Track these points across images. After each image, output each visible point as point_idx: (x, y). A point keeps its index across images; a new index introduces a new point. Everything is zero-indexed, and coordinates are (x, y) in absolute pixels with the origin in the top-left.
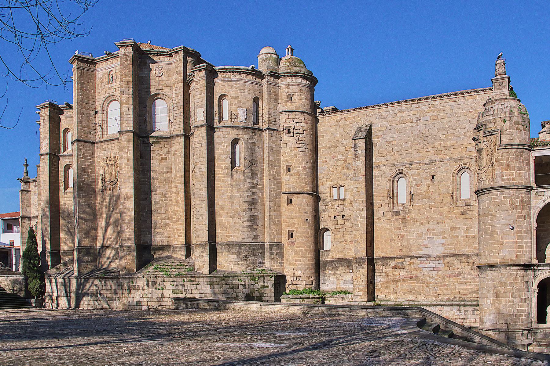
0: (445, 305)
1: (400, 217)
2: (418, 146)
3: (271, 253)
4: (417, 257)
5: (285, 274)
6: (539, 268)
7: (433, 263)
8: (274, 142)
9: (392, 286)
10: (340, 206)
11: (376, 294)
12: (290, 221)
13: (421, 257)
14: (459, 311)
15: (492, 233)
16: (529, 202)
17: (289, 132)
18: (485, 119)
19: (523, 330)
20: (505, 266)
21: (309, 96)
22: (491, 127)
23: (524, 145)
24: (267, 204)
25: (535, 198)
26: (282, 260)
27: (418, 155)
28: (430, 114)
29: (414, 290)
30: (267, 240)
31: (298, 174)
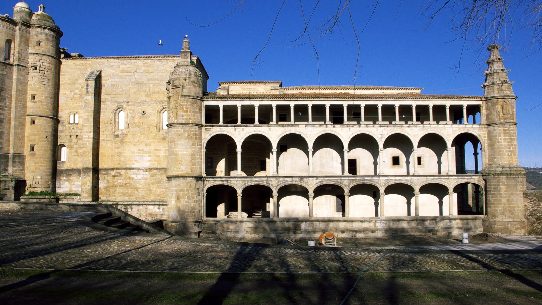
0: (149, 205)
1: (119, 139)
2: (134, 90)
3: (14, 162)
4: (131, 169)
5: (26, 179)
6: (207, 179)
7: (142, 174)
8: (22, 75)
9: (112, 190)
10: (75, 128)
11: (100, 196)
12: (32, 137)
13: (133, 169)
14: (159, 209)
15: (175, 154)
16: (201, 135)
17: (36, 69)
18: (174, 77)
19: (195, 222)
20: (183, 177)
21: (55, 44)
22: (176, 83)
23: (198, 97)
24: (13, 123)
25: (205, 133)
26: (24, 167)
27: (134, 96)
28: (144, 69)
29: (127, 193)
30: (11, 151)
31: (41, 102)
